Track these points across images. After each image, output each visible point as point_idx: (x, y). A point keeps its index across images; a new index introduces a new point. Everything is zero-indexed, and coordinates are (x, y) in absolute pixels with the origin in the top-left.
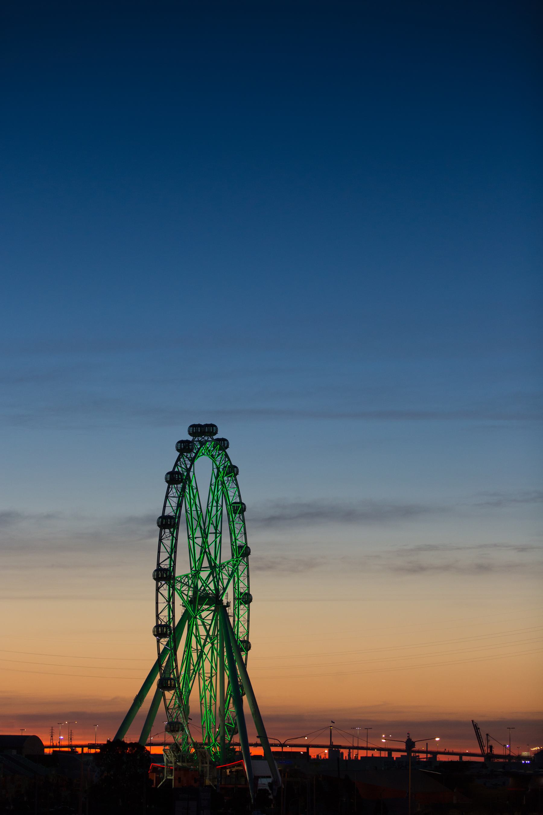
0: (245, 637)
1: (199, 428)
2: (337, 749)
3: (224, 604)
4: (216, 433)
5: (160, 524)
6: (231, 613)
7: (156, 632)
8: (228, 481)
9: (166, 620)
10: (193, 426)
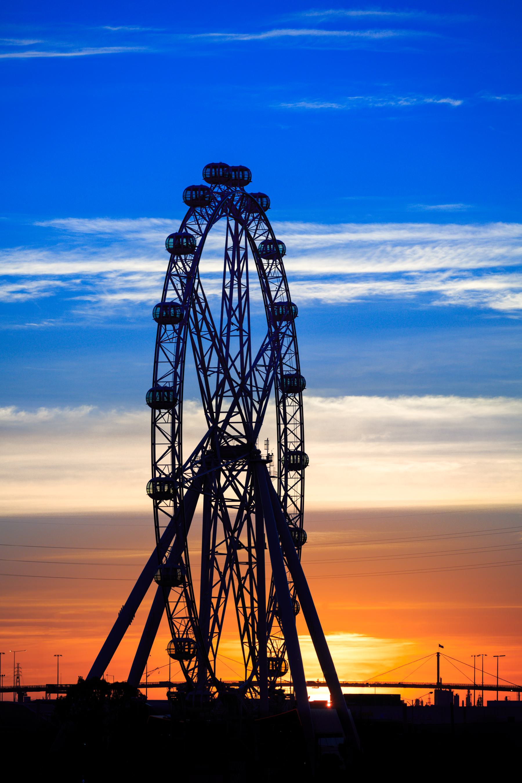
0: (297, 521)
1: (221, 170)
2: (448, 690)
3: (262, 458)
4: (249, 181)
5: (158, 316)
6: (274, 472)
7: (151, 490)
8: (268, 266)
9: (167, 471)
10: (211, 166)
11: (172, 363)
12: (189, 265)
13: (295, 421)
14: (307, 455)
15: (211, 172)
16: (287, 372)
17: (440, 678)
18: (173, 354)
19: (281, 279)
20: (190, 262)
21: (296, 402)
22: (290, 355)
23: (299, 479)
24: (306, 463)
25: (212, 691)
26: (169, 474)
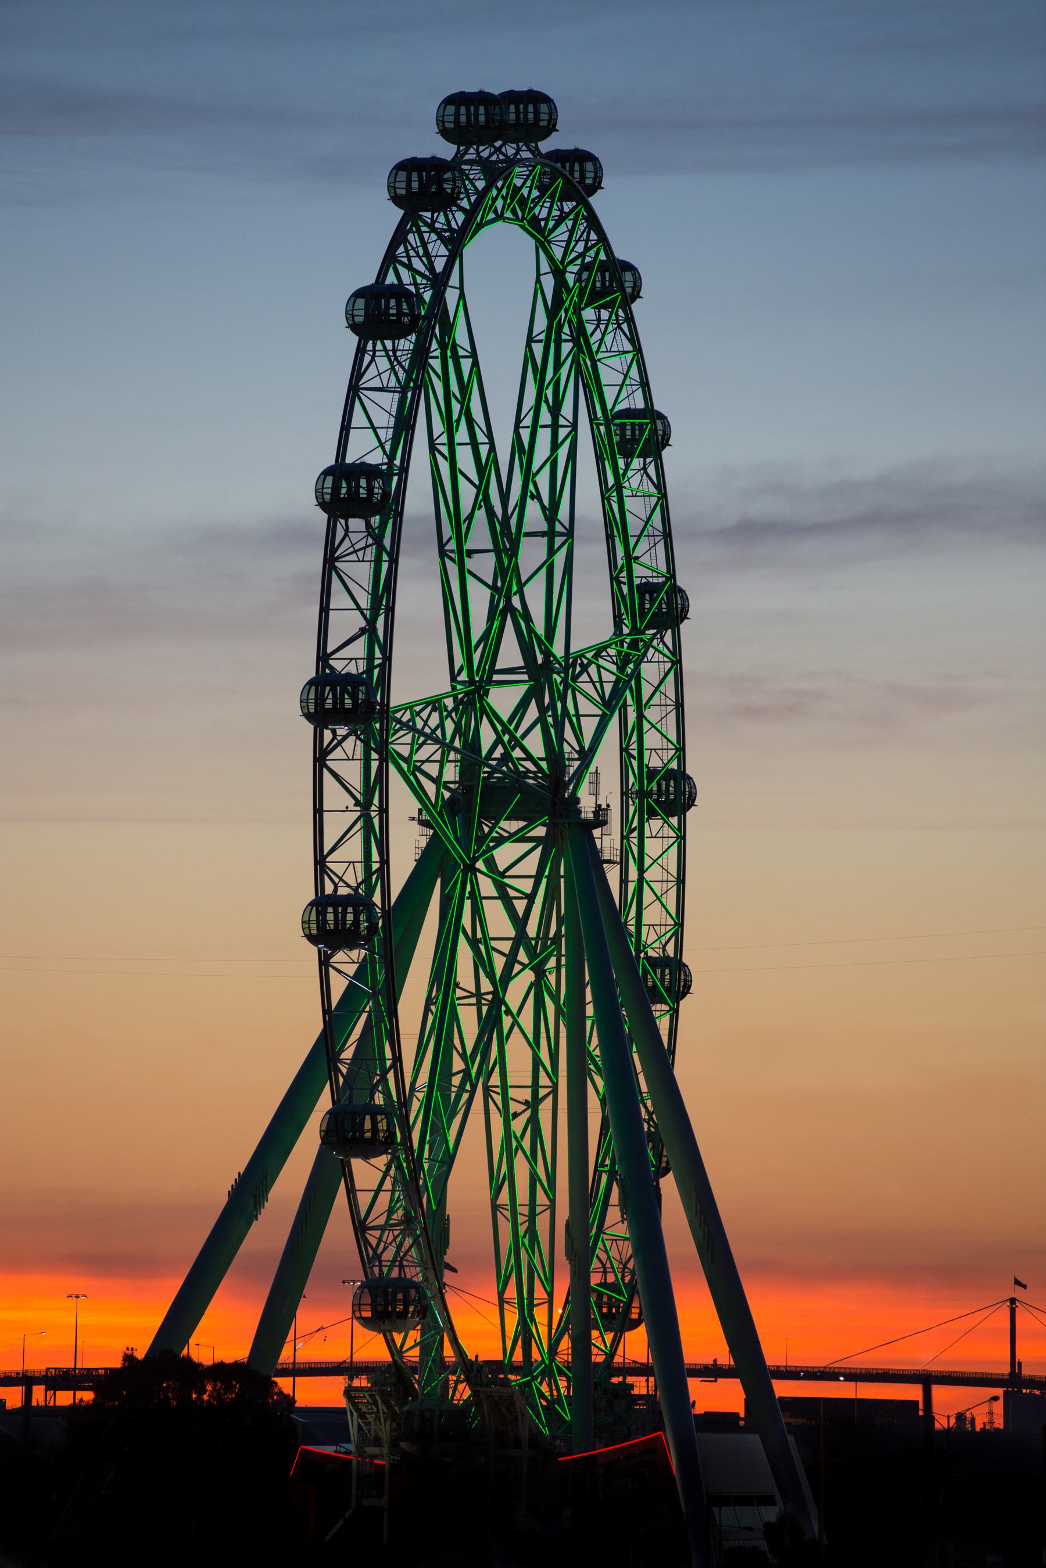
0: (667, 943)
1: (482, 110)
3: (583, 816)
4: (551, 128)
5: (327, 497)
7: (314, 926)
8: (598, 326)
10: (457, 100)
11: (365, 611)
12: (404, 363)
13: (663, 697)
14: (687, 966)
15: (457, 114)
16: (643, 578)
17: (1017, 1361)
18: (366, 591)
19: (630, 356)
20: (405, 357)
21: (665, 655)
22: (651, 538)
23: (672, 841)
24: (689, 798)
25: (461, 1399)
26: (356, 885)
